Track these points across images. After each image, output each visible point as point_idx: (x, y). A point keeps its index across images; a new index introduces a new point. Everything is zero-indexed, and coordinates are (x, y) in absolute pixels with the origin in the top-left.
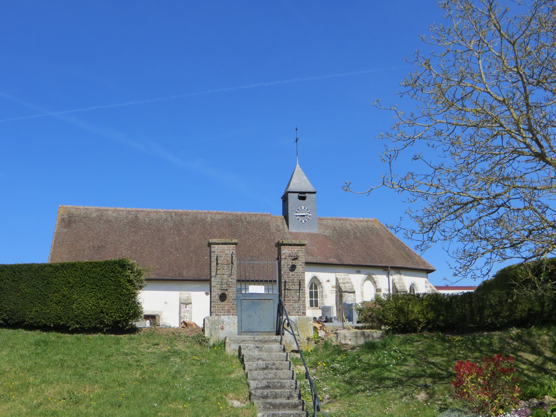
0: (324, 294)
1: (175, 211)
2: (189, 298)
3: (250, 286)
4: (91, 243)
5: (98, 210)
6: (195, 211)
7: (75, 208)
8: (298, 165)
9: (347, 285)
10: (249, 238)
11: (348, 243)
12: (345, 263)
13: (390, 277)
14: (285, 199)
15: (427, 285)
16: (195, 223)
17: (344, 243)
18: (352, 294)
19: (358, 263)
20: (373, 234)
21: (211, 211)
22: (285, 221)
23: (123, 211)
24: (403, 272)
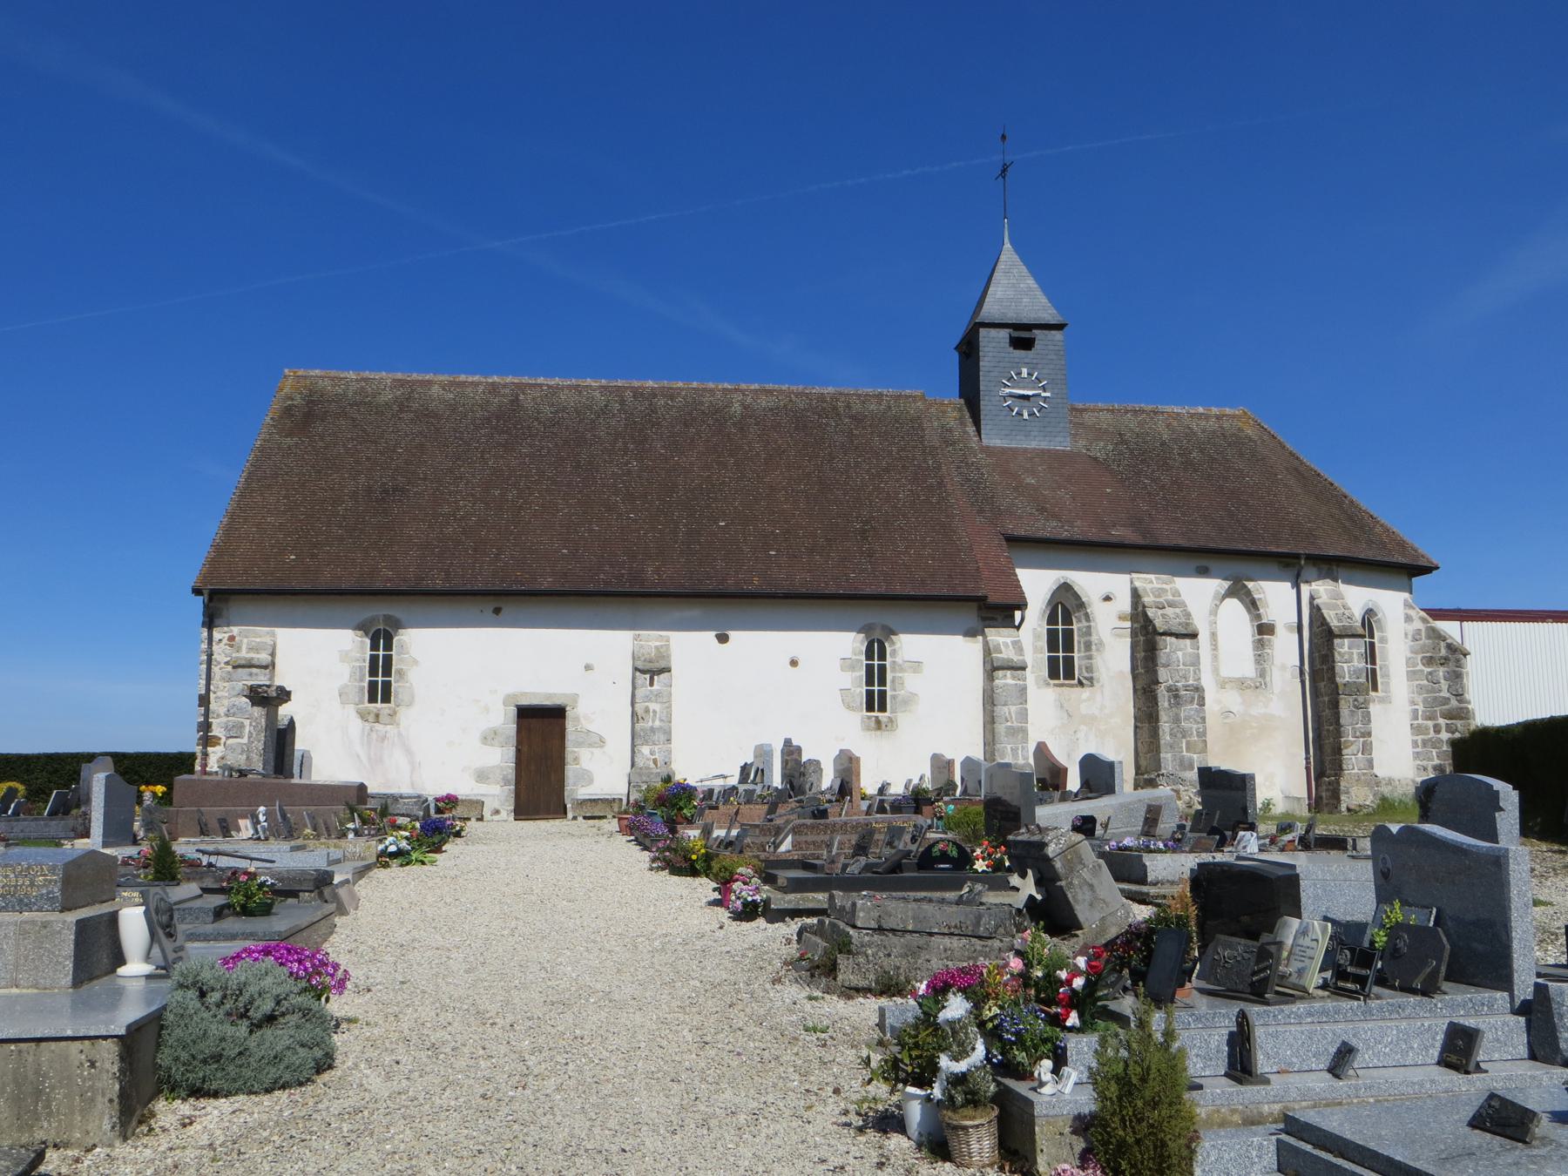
0: (1094, 638)
1: (636, 384)
2: (664, 654)
3: (1094, 1108)
4: (362, 479)
5: (401, 383)
6: (695, 384)
7: (332, 379)
8: (1007, 245)
9: (1169, 611)
10: (857, 465)
11: (1165, 479)
12: (1165, 542)
13: (1305, 588)
14: (969, 350)
15: (1412, 613)
16: (694, 419)
17: (1153, 480)
18: (1188, 642)
19: (1202, 543)
20: (1241, 455)
21: (743, 386)
22: (967, 415)
23: (476, 384)
24: (1342, 571)
